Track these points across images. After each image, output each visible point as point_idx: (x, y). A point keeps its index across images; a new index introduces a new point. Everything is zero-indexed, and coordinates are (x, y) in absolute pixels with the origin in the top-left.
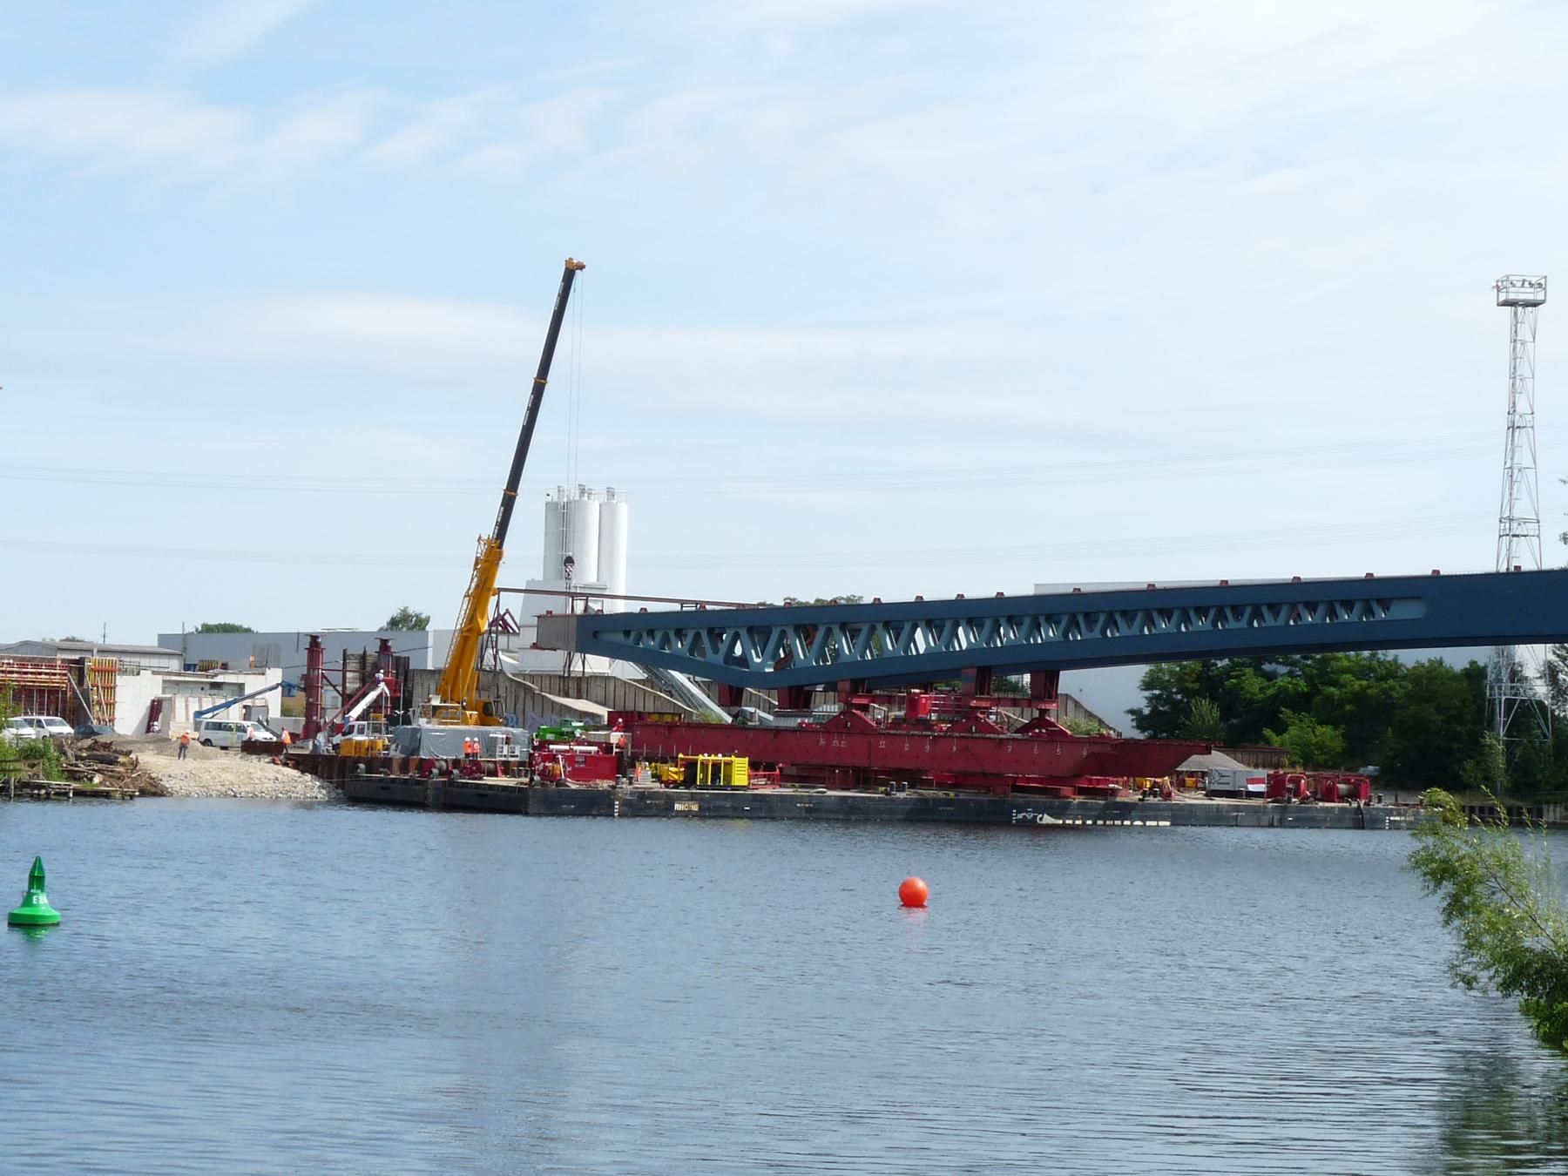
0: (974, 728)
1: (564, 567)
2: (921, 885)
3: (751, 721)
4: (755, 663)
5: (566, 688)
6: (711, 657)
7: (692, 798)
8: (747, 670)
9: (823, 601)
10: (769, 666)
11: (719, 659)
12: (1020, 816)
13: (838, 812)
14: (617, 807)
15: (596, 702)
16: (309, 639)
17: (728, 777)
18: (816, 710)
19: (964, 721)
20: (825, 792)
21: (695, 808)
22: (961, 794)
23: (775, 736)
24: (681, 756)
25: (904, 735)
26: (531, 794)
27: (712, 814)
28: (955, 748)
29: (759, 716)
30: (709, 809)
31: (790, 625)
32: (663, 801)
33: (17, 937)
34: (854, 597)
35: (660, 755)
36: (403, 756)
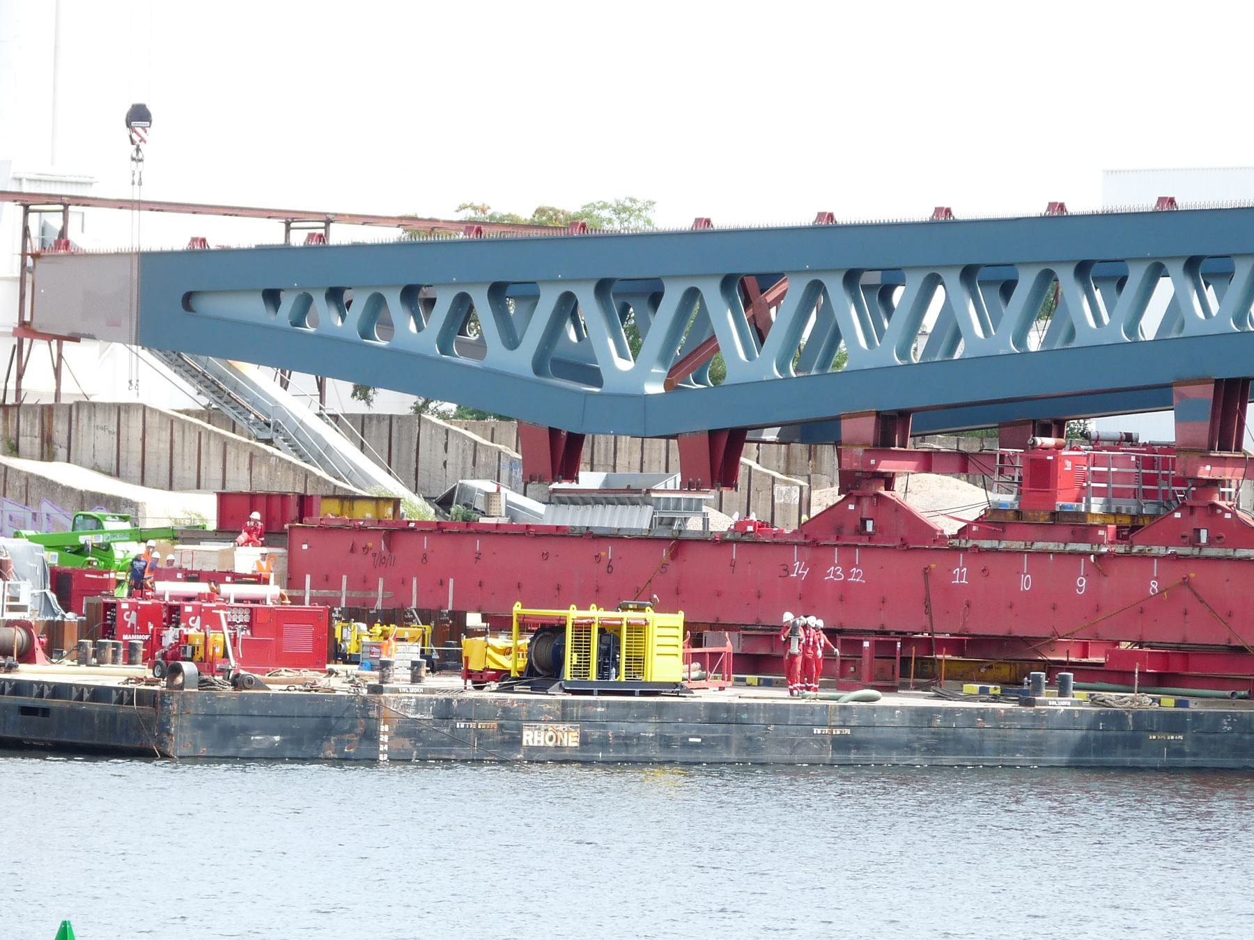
0: (1204, 534)
1: (128, 131)
3: (484, 514)
4: (620, 372)
5: (12, 433)
6: (498, 355)
7: (564, 714)
8: (597, 390)
9: (556, 212)
10: (654, 378)
11: (521, 360)
13: (909, 748)
14: (384, 738)
15: (96, 468)
17: (637, 661)
18: (661, 486)
19: (1178, 515)
20: (875, 699)
21: (571, 739)
22: (1192, 701)
23: (674, 556)
24: (517, 608)
25: (1021, 552)
26: (174, 708)
27: (612, 755)
28: (1154, 585)
29: (508, 502)
30: (604, 744)
31: (587, 280)
32: (494, 724)
34: (633, 200)
35: (379, 605)
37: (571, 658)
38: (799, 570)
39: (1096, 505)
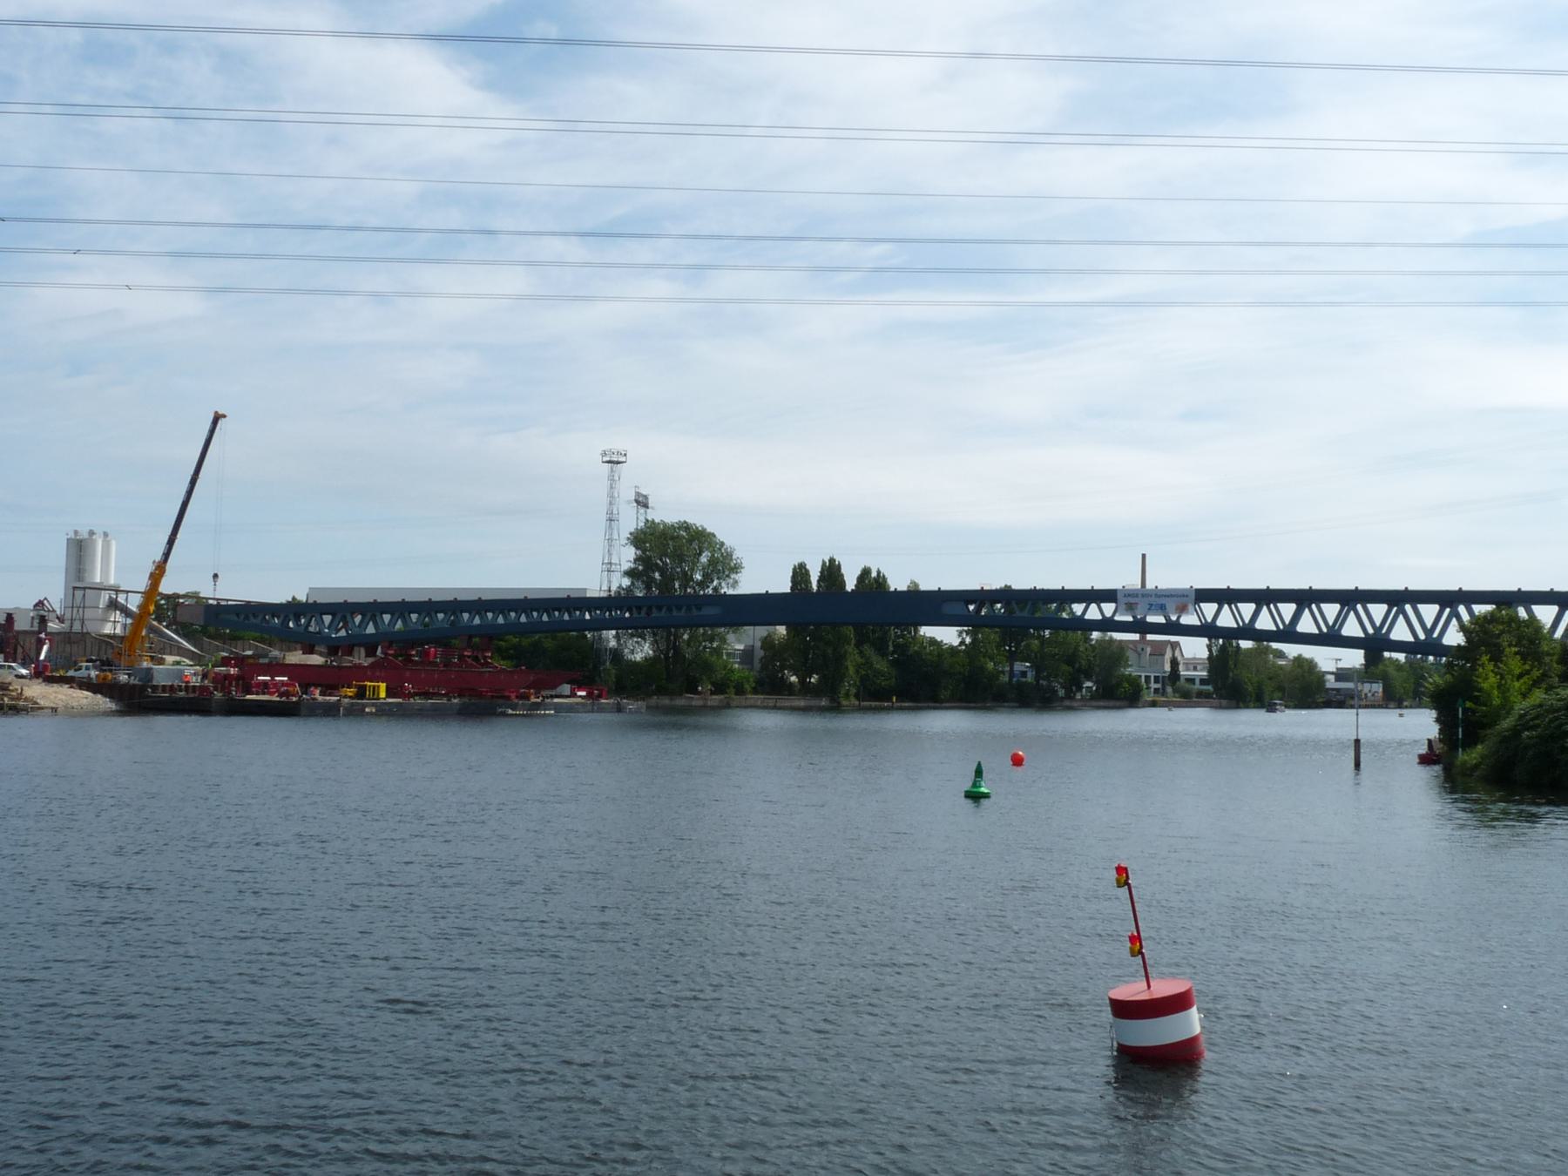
2: (1021, 753)
7: (373, 705)
12: (500, 710)
16: (5, 615)
17: (378, 694)
21: (374, 710)
25: (434, 670)
33: (969, 803)
36: (140, 683)
37: (368, 693)
38: (369, 673)
39: (438, 660)
